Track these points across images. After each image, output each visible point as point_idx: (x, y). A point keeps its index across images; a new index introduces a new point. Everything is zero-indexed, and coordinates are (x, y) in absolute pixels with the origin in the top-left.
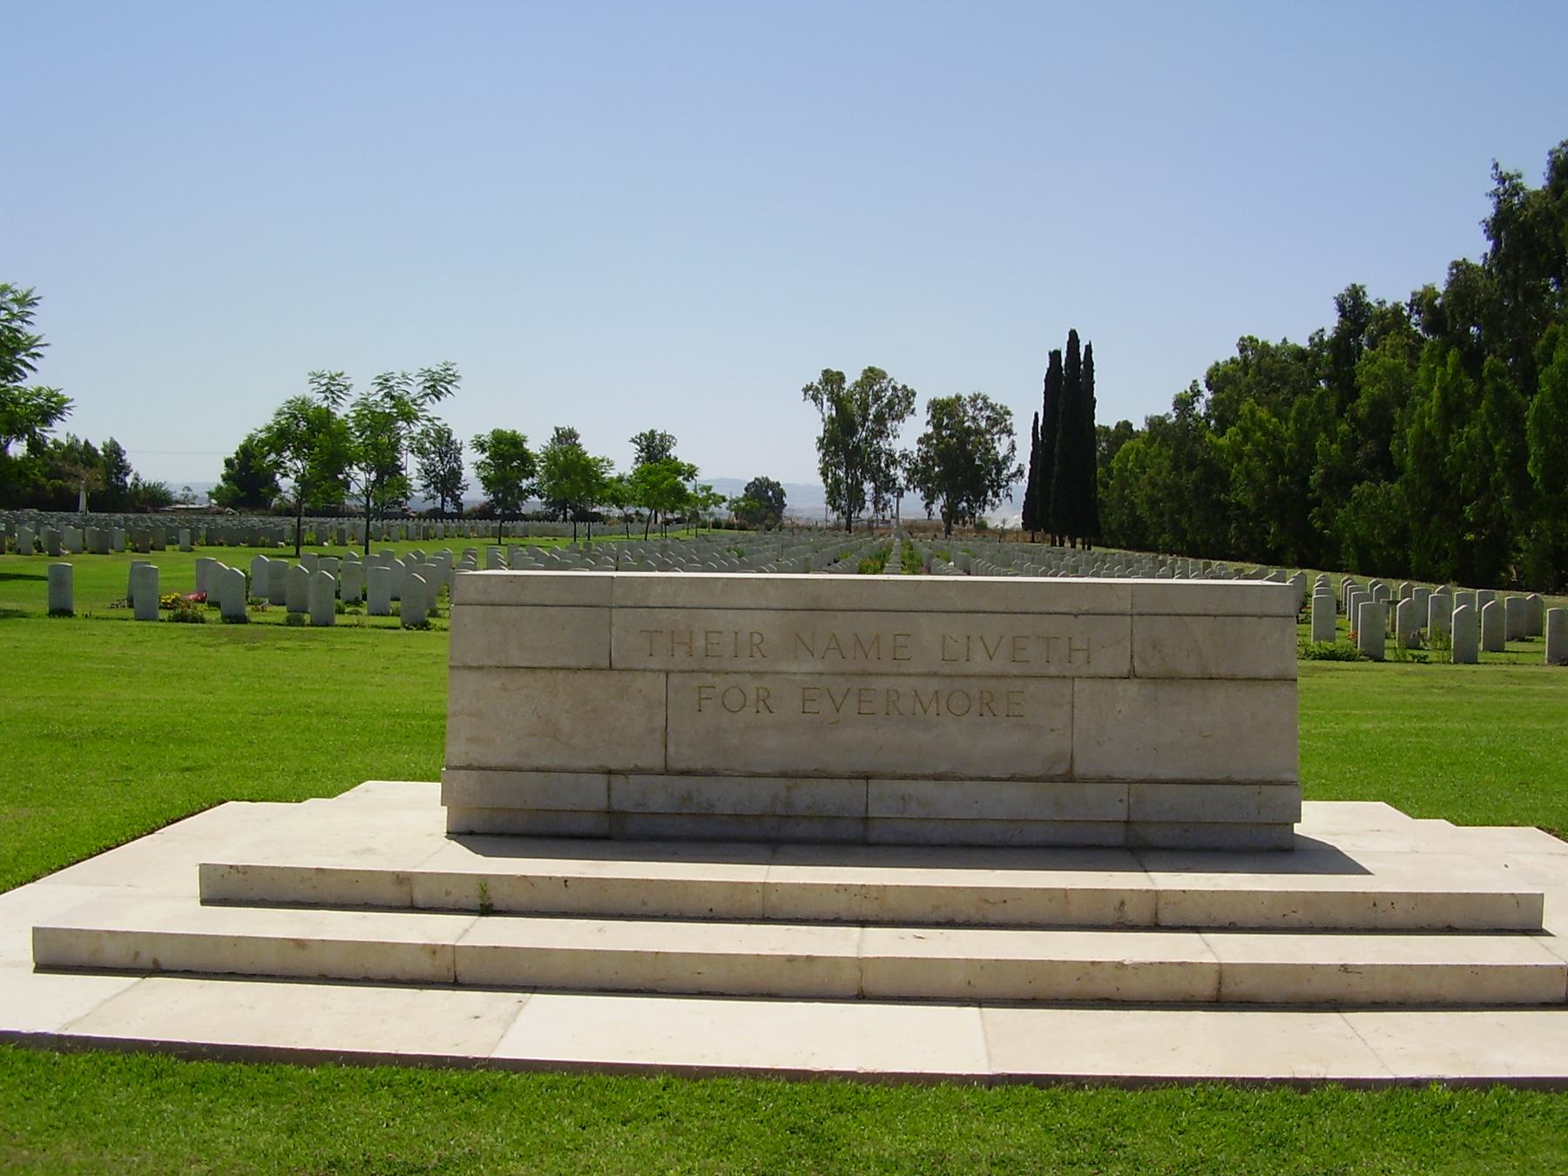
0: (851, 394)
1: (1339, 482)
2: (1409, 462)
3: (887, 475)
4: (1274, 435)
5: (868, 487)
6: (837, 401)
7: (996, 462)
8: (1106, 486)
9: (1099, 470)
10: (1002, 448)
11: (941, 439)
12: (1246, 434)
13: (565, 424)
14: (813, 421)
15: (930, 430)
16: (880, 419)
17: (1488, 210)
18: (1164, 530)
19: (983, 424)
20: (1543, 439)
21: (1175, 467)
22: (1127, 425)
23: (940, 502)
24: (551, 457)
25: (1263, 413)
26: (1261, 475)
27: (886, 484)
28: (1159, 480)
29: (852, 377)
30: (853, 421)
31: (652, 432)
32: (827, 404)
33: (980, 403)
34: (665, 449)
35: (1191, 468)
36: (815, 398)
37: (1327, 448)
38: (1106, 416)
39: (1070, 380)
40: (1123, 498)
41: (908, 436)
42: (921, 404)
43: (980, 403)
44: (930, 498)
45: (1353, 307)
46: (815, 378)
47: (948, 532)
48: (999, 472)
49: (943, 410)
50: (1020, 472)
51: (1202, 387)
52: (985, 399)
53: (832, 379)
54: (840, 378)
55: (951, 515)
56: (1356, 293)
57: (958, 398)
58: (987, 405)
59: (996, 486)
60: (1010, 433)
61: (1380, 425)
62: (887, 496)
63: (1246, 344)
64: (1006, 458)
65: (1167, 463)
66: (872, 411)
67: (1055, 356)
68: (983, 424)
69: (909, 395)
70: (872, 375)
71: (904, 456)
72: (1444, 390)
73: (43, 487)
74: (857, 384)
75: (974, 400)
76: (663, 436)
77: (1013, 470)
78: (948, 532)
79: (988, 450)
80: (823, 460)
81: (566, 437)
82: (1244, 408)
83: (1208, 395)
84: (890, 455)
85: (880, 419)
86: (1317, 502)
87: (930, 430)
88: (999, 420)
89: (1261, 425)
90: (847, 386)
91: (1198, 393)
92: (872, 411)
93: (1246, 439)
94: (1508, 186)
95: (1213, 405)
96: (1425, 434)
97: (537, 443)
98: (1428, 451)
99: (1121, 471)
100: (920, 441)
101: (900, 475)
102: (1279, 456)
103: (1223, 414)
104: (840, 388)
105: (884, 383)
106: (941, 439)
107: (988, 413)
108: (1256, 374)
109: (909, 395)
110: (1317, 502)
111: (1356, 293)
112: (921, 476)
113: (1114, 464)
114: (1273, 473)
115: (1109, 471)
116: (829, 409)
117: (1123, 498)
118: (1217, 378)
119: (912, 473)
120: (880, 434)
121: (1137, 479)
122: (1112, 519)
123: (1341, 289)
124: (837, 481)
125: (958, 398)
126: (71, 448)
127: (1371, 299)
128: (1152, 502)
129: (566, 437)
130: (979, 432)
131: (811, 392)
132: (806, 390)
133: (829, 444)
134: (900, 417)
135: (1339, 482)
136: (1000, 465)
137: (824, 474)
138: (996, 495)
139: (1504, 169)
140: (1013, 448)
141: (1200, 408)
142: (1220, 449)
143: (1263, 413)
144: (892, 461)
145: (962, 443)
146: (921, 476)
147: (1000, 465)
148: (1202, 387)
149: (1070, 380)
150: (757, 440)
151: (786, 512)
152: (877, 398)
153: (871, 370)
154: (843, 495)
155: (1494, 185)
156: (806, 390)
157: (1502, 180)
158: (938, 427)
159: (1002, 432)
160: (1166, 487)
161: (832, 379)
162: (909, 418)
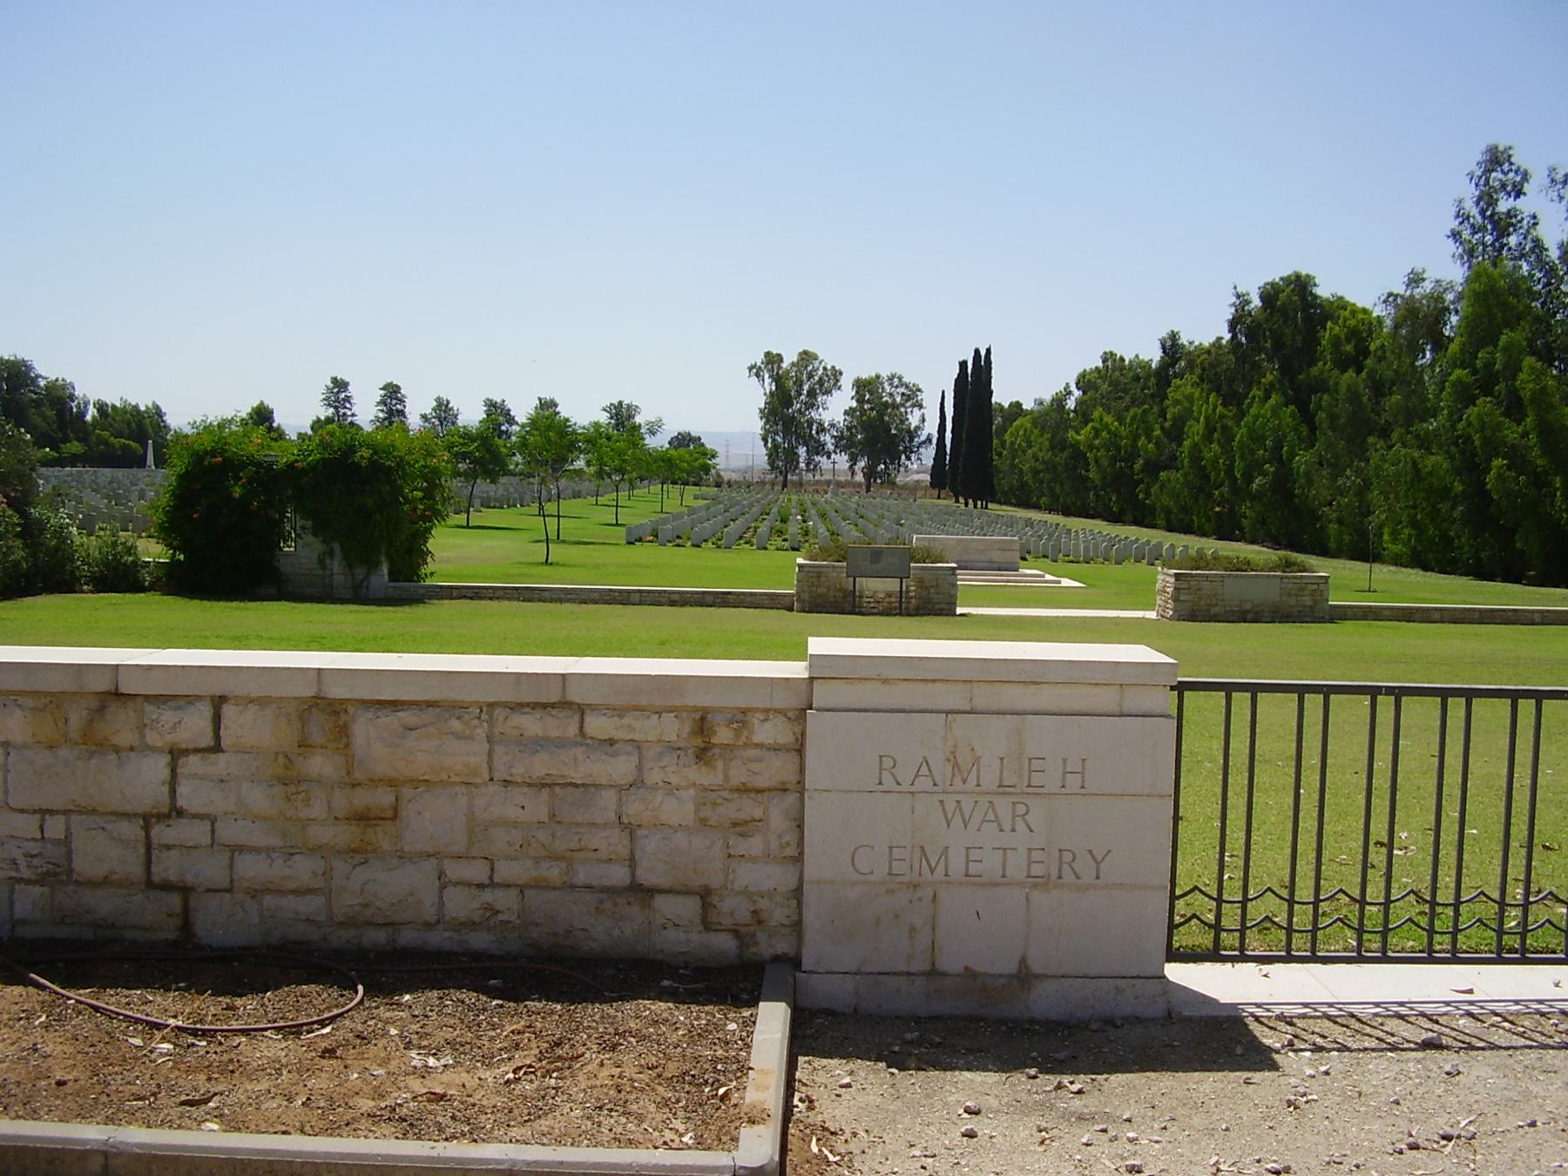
0: (788, 372)
1: (1153, 468)
2: (1186, 462)
3: (819, 441)
4: (1115, 435)
5: (802, 451)
6: (778, 379)
7: (909, 431)
8: (1000, 455)
9: (995, 441)
10: (914, 420)
11: (863, 412)
12: (1097, 433)
13: (547, 396)
14: (757, 394)
15: (854, 404)
16: (812, 394)
17: (1229, 313)
18: (1043, 495)
19: (898, 399)
20: (1243, 458)
21: (1052, 447)
22: (1018, 405)
23: (862, 464)
24: (534, 422)
25: (1108, 419)
26: (1105, 462)
27: (817, 448)
28: (1040, 455)
29: (790, 358)
30: (789, 393)
31: (620, 403)
32: (767, 380)
33: (896, 381)
34: (631, 417)
35: (1063, 450)
36: (757, 375)
37: (1147, 447)
38: (1002, 394)
39: (974, 381)
40: (1013, 466)
41: (835, 408)
42: (847, 382)
43: (896, 381)
44: (853, 460)
45: (1172, 347)
46: (759, 359)
47: (868, 490)
48: (911, 440)
49: (865, 388)
50: (929, 440)
51: (1073, 388)
52: (900, 379)
53: (773, 360)
54: (780, 358)
55: (870, 474)
56: (1174, 336)
57: (878, 377)
58: (902, 384)
59: (909, 451)
60: (921, 407)
61: (1176, 433)
62: (817, 458)
63: (1107, 357)
64: (918, 428)
65: (1047, 444)
66: (806, 387)
67: (963, 364)
68: (898, 399)
69: (836, 374)
70: (806, 357)
71: (833, 426)
72: (1207, 418)
73: (113, 445)
74: (793, 364)
75: (891, 379)
76: (629, 406)
77: (923, 438)
78: (868, 490)
79: (902, 422)
80: (763, 428)
81: (547, 405)
82: (1096, 415)
83: (1077, 393)
84: (820, 424)
85: (812, 394)
86: (1141, 481)
87: (854, 404)
88: (912, 396)
89: (1106, 426)
90: (784, 365)
91: (1070, 393)
92: (806, 387)
93: (1097, 436)
94: (1242, 300)
95: (1079, 402)
96: (1196, 445)
97: (522, 411)
98: (1196, 456)
99: (1013, 443)
100: (846, 413)
101: (828, 439)
102: (1118, 448)
103: (1083, 411)
104: (779, 368)
105: (816, 364)
106: (863, 412)
107: (902, 390)
108: (1112, 383)
109: (836, 374)
110: (1141, 481)
111: (1174, 336)
112: (845, 442)
113: (1007, 437)
114: (1114, 460)
115: (1003, 443)
116: (770, 385)
117: (1013, 466)
118: (1084, 382)
119: (838, 439)
120: (811, 406)
121: (1024, 452)
122: (1004, 482)
123: (1164, 334)
124: (776, 446)
125: (878, 377)
126: (124, 411)
127: (1184, 340)
128: (1035, 472)
129: (547, 405)
130: (895, 406)
131: (756, 371)
132: (750, 369)
133: (770, 413)
134: (828, 392)
135: (1153, 468)
136: (912, 434)
137: (765, 440)
138: (909, 458)
139: (1239, 290)
140: (923, 420)
141: (1071, 404)
142: (1078, 442)
143: (1108, 419)
144: (821, 429)
145: (881, 415)
146: (845, 442)
147: (912, 434)
148: (1073, 388)
149: (974, 381)
150: (726, 417)
151: (720, 462)
152: (810, 376)
153: (805, 352)
154: (782, 460)
155: (1234, 299)
156: (750, 369)
157: (1238, 297)
158: (861, 401)
159: (913, 406)
160: (1044, 462)
161: (773, 360)
162: (835, 393)
